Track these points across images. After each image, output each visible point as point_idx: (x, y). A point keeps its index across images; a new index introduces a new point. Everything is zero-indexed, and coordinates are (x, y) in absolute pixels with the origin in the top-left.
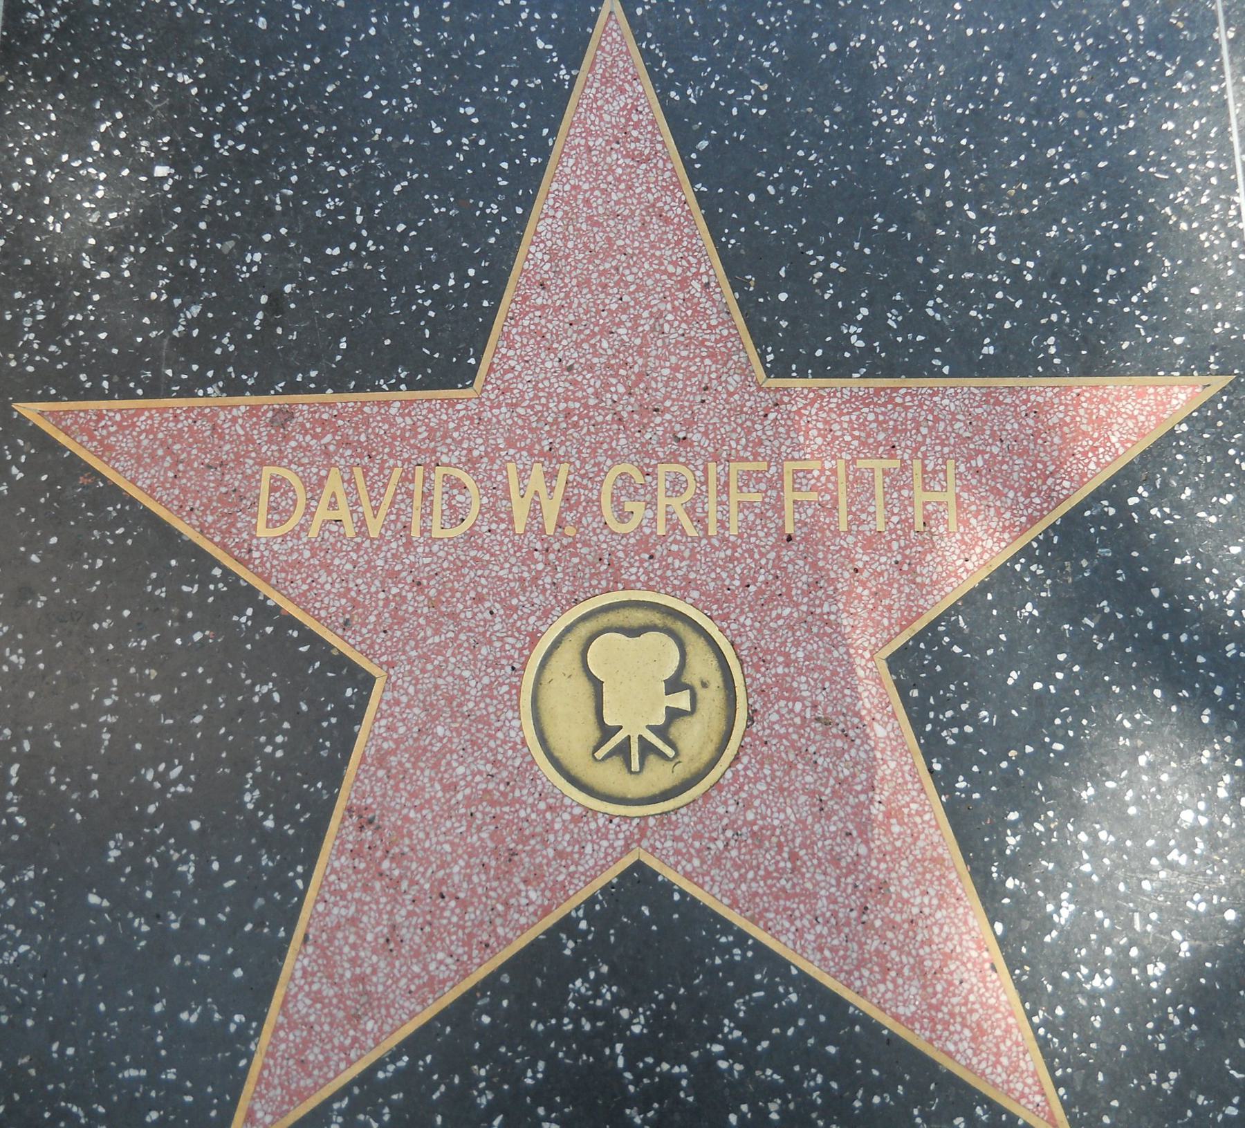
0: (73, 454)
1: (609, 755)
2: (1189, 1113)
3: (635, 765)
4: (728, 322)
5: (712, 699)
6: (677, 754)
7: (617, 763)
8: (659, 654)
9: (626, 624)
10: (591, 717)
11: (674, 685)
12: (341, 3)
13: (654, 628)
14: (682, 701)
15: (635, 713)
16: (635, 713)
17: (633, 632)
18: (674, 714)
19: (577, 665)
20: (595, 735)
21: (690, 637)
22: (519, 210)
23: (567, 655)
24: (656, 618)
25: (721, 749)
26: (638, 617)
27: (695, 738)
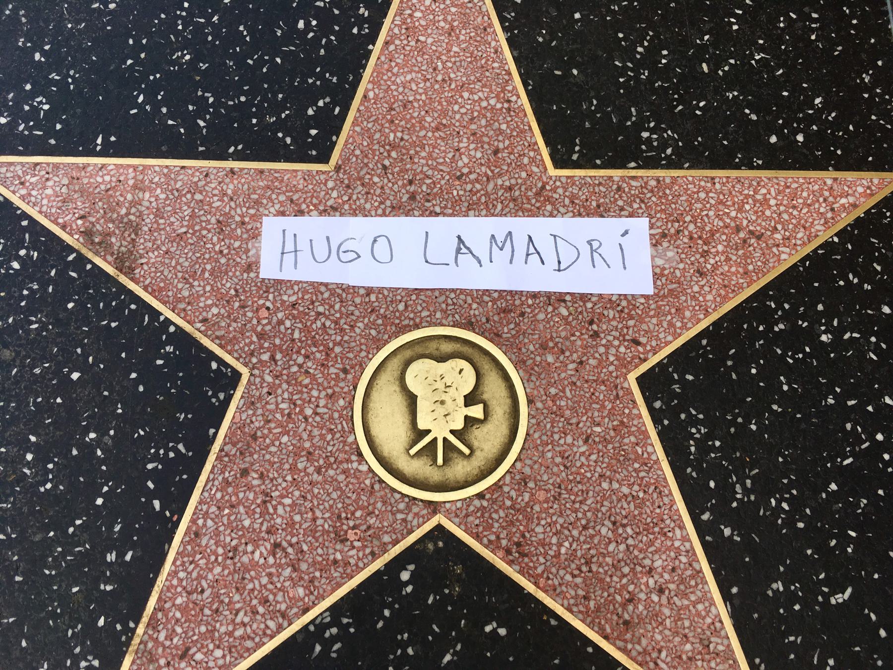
0: (682, 168)
1: (419, 454)
4: (246, 440)
5: (500, 411)
8: (460, 376)
9: (435, 353)
11: (470, 400)
14: (477, 411)
15: (439, 425)
16: (439, 425)
18: (469, 421)
19: (397, 374)
21: (486, 366)
22: (706, 517)
24: (456, 347)
26: (447, 347)
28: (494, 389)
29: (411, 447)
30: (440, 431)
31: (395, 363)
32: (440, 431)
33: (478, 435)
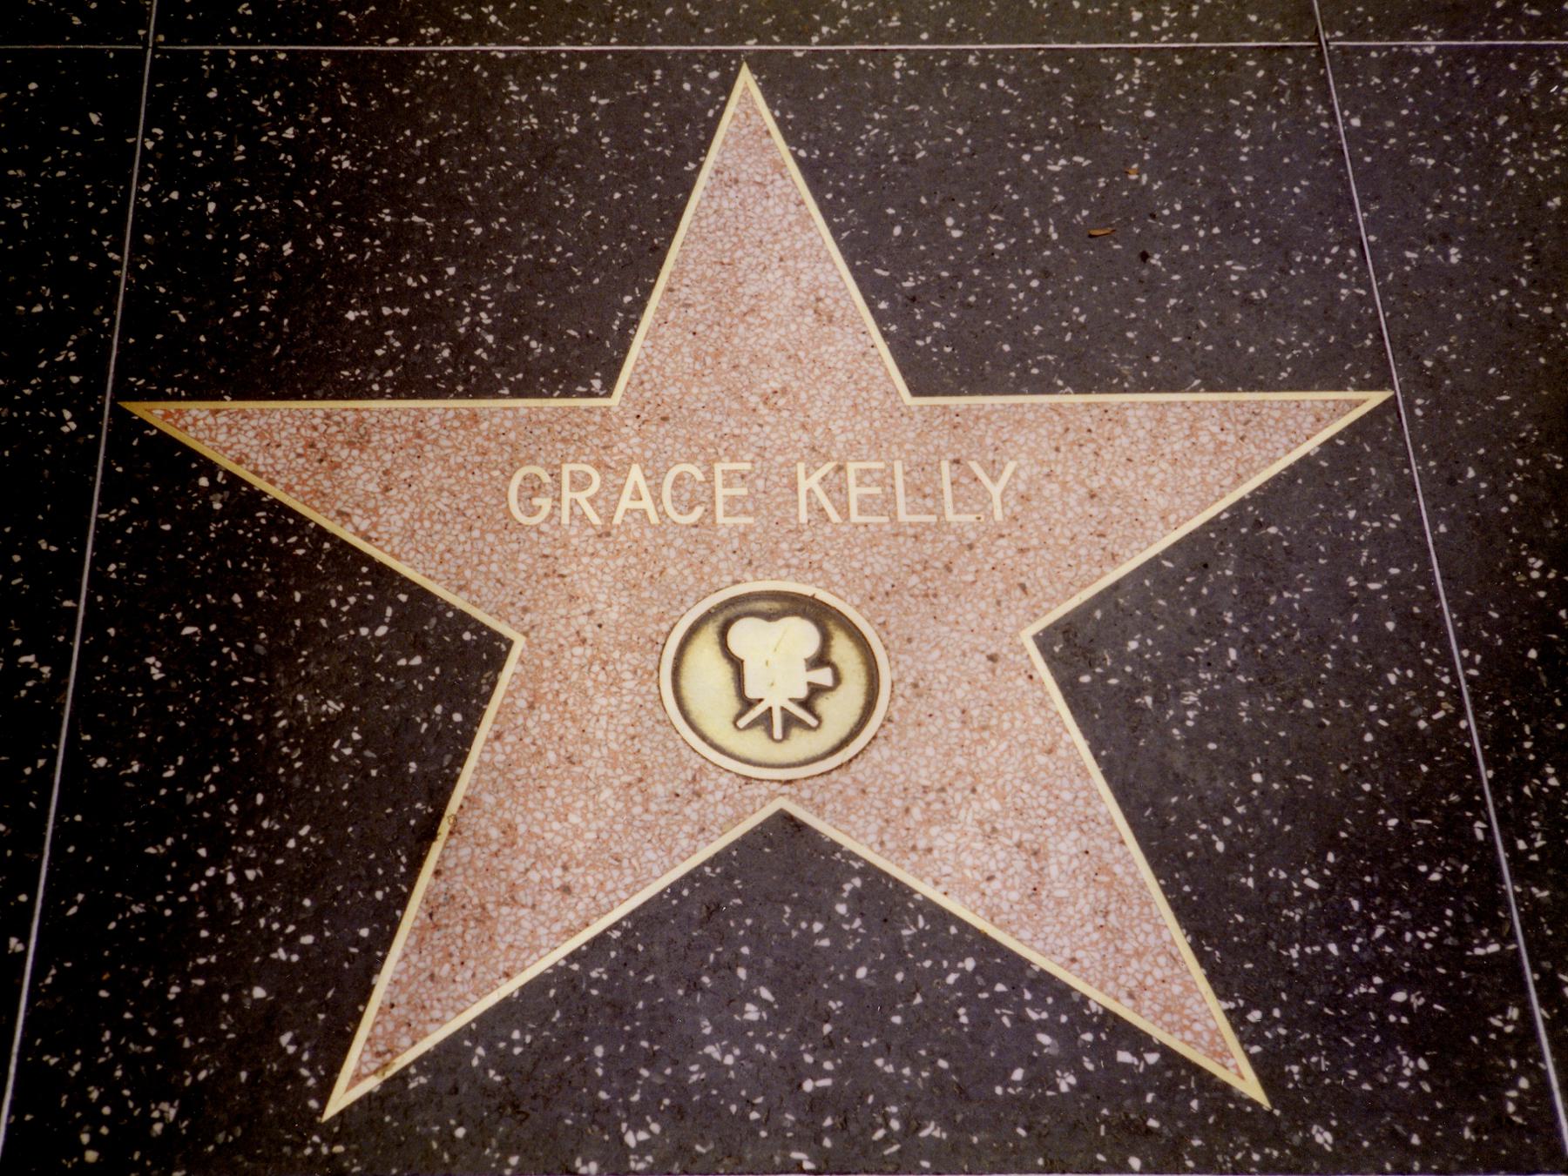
1: (750, 726)
2: (1549, 932)
3: (778, 733)
6: (750, 726)
7: (758, 734)
8: (801, 635)
10: (730, 690)
11: (821, 660)
12: (4, 95)
13: (738, 617)
17: (770, 617)
20: (734, 706)
23: (709, 634)
25: (704, 738)
26: (763, 606)
27: (840, 709)
28: (843, 651)
29: (740, 715)
33: (823, 704)
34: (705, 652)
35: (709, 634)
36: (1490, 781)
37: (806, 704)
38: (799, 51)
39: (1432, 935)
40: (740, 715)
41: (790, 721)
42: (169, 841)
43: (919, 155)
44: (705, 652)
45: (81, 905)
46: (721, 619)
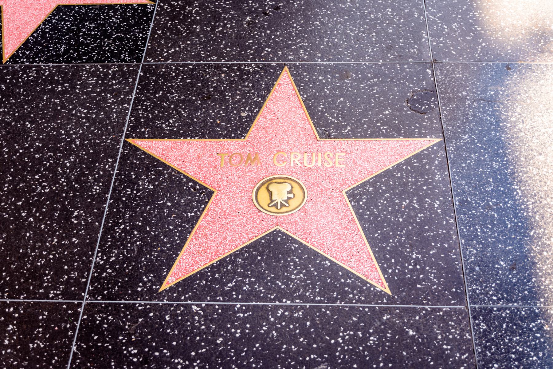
1: (272, 206)
10: (269, 198)
11: (289, 193)
13: (271, 183)
14: (291, 196)
18: (289, 198)
20: (269, 202)
23: (264, 189)
25: (260, 206)
29: (270, 204)
30: (279, 201)
31: (266, 185)
32: (279, 201)
33: (291, 202)
34: (263, 191)
35: (264, 189)
36: (106, 204)
37: (286, 201)
38: (161, 303)
39: (531, 359)
40: (270, 204)
41: (282, 205)
42: (308, 359)
43: (133, 340)
44: (263, 191)
45: (283, 348)
46: (266, 185)
